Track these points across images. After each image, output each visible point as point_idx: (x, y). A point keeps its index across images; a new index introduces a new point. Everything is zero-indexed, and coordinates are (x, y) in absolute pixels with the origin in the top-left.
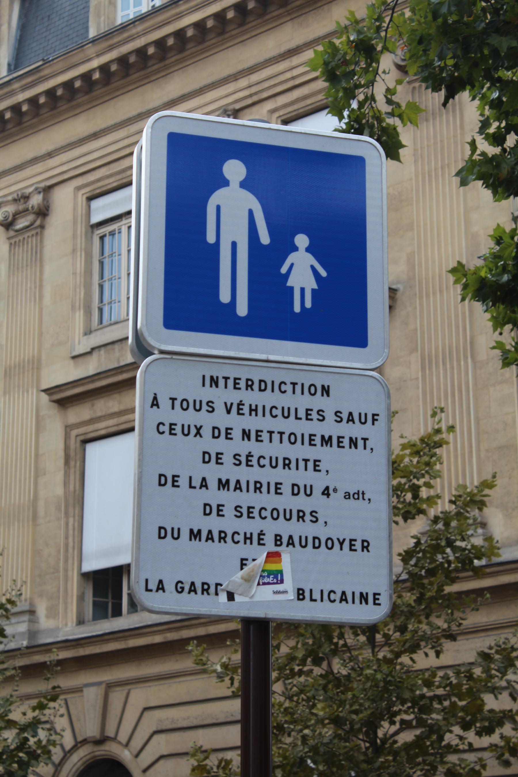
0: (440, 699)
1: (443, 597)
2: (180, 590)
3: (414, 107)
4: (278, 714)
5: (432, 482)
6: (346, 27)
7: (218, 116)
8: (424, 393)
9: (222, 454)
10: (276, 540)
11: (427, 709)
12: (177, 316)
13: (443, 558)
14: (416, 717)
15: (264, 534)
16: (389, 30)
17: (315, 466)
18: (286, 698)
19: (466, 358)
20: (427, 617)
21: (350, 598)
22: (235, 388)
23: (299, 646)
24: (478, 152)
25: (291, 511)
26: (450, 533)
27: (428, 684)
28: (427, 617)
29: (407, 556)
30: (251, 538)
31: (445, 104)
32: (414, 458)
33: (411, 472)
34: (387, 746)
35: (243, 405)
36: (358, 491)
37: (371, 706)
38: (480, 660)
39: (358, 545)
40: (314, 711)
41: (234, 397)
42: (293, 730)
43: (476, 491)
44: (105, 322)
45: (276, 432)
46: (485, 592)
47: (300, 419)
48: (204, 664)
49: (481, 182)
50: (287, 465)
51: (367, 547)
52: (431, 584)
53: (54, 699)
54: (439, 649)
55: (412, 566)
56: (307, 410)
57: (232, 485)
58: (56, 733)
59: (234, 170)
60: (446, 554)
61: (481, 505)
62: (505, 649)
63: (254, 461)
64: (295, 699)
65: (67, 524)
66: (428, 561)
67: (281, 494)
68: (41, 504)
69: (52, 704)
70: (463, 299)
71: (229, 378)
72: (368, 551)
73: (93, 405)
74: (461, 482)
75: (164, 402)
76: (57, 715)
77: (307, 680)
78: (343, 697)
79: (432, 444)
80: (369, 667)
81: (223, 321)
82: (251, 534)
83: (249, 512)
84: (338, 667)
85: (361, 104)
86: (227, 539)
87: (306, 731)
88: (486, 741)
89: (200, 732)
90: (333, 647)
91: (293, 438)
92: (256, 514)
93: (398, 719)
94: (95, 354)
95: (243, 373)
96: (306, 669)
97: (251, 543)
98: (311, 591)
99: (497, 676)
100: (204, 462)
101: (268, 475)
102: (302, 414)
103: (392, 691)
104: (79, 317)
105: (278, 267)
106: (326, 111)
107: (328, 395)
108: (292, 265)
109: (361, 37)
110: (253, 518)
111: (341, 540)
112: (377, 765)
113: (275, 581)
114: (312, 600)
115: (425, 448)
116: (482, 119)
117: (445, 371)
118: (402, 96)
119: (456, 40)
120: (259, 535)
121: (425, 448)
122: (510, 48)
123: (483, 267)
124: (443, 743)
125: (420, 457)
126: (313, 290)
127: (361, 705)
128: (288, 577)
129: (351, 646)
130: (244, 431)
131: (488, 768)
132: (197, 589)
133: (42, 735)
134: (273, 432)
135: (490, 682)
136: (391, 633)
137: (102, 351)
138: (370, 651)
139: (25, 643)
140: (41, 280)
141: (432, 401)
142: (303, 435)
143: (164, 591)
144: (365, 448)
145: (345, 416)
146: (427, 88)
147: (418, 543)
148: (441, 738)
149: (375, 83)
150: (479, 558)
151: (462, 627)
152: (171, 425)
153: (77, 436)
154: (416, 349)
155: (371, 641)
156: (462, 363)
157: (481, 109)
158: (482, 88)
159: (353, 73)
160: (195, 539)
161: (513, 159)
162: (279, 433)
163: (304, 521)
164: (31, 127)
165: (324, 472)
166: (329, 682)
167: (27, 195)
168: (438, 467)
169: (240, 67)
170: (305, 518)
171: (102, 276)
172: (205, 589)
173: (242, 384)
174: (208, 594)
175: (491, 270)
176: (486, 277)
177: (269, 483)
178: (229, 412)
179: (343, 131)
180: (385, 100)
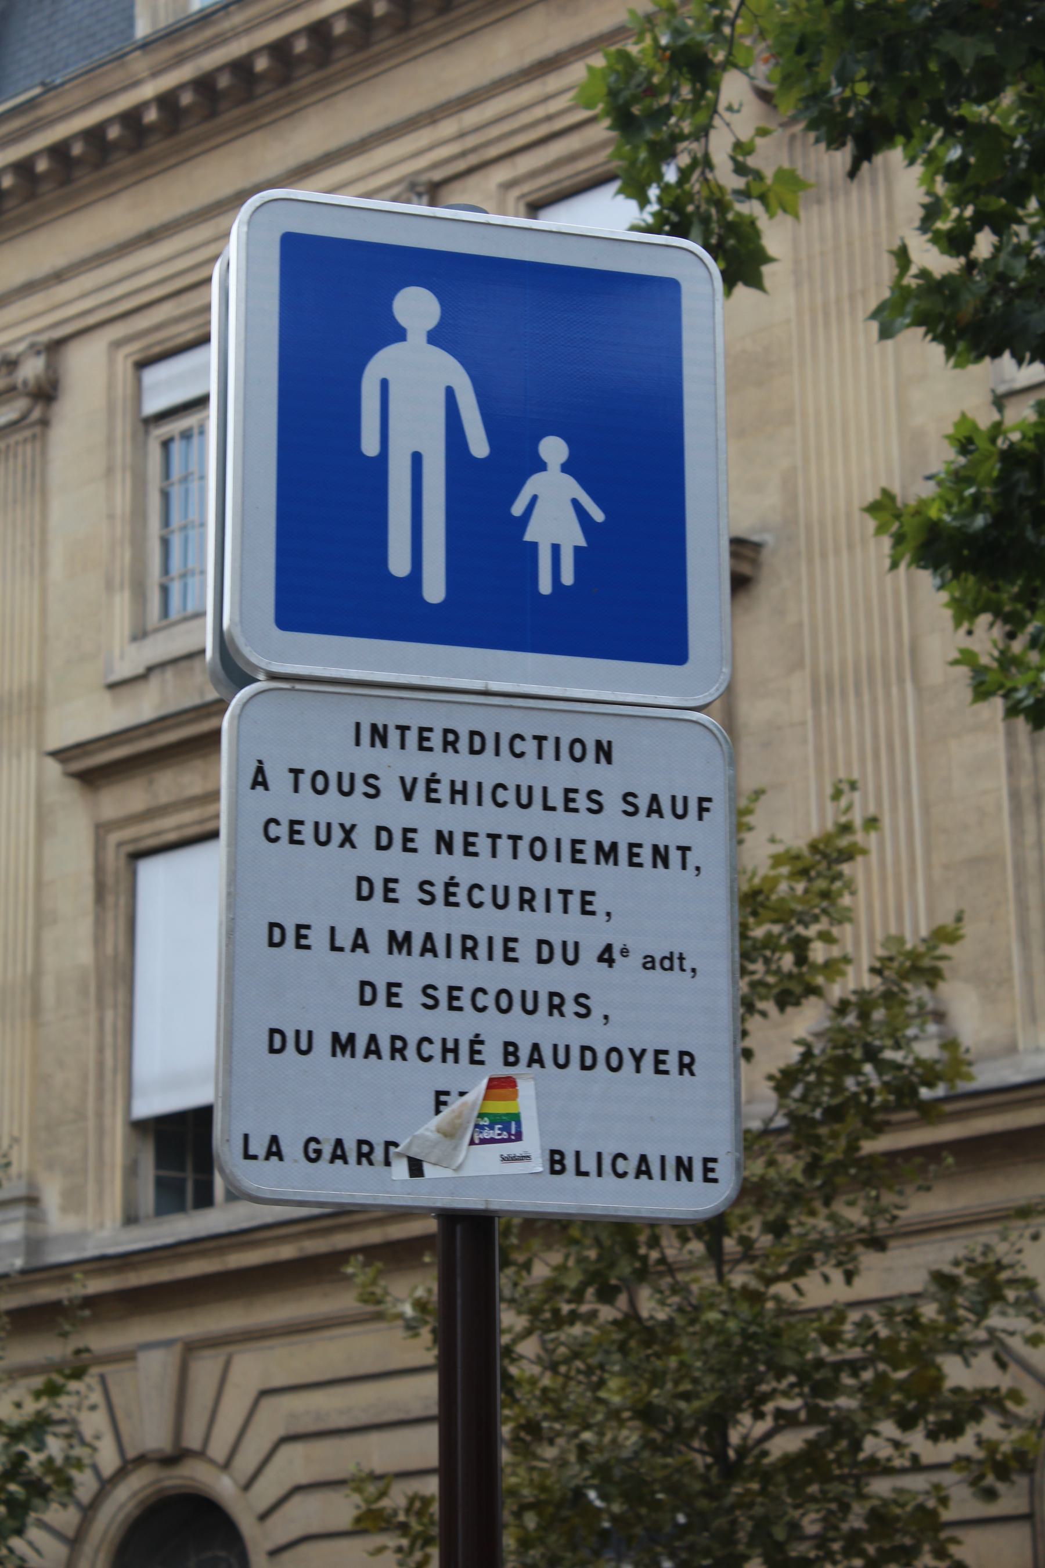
0: (854, 1367)
1: (858, 1162)
2: (313, 1156)
3: (789, 179)
4: (529, 1401)
5: (835, 931)
6: (649, 19)
7: (395, 199)
8: (819, 752)
9: (396, 881)
10: (507, 1054)
11: (829, 1388)
12: (301, 604)
13: (859, 1084)
14: (806, 1405)
15: (482, 1042)
16: (739, 22)
17: (584, 903)
18: (545, 1368)
19: (901, 680)
20: (827, 1203)
21: (655, 1169)
22: (421, 748)
23: (571, 1263)
24: (914, 270)
25: (536, 993)
26: (872, 1034)
27: (831, 1337)
28: (827, 1203)
29: (784, 1081)
30: (455, 1051)
31: (853, 173)
32: (798, 881)
33: (792, 913)
34: (749, 1461)
35: (438, 781)
36: (672, 953)
37: (718, 1385)
38: (933, 1288)
39: (672, 1062)
40: (602, 1394)
41: (419, 765)
42: (559, 1434)
43: (922, 949)
44: (175, 612)
45: (505, 837)
46: (944, 1154)
47: (553, 809)
48: (379, 1302)
49: (922, 330)
50: (527, 900)
51: (689, 1066)
52: (835, 1135)
53: (78, 1374)
54: (850, 1266)
55: (796, 1100)
56: (567, 791)
57: (417, 943)
58: (83, 1443)
59: (417, 307)
60: (864, 1074)
61: (932, 976)
62: (984, 1266)
63: (461, 896)
64: (563, 1369)
65: (101, 1022)
66: (827, 1090)
67: (516, 960)
68: (48, 983)
69: (73, 1385)
70: (894, 565)
71: (408, 728)
72: (692, 1074)
73: (151, 782)
74: (893, 931)
75: (278, 777)
76: (85, 1408)
77: (587, 1334)
78: (658, 1364)
79: (835, 855)
80: (712, 1306)
81: (392, 612)
82: (456, 1041)
83: (451, 998)
84: (650, 1306)
85: (684, 175)
86: (406, 1053)
87: (587, 1436)
88: (946, 1450)
89: (374, 1438)
90: (637, 1265)
91: (538, 848)
92: (465, 1001)
93: (769, 1407)
94: (154, 681)
95: (438, 717)
96: (584, 1308)
97: (456, 1061)
98: (578, 1154)
99: (968, 1320)
100: (360, 898)
101: (487, 923)
102: (556, 799)
103: (760, 1351)
104: (122, 604)
105: (510, 504)
106: (616, 185)
107: (609, 761)
108: (534, 499)
109: (682, 41)
110: (460, 1009)
111: (638, 1052)
112: (729, 1500)
113: (505, 1135)
114: (580, 1173)
115: (819, 862)
116: (927, 200)
117: (860, 707)
118: (768, 158)
119: (872, 45)
120: (472, 1043)
121: (819, 862)
122: (981, 60)
123: (933, 500)
124: (862, 1456)
125: (810, 880)
126: (577, 550)
127: (695, 1381)
128: (530, 1127)
129: (675, 1262)
130: (440, 834)
131: (952, 1504)
132: (348, 1154)
133: (55, 1446)
134: (499, 836)
135: (954, 1331)
136: (754, 1234)
137: (169, 674)
138: (712, 1271)
139: (19, 1263)
140: (44, 531)
141: (834, 768)
142: (558, 841)
143: (281, 1159)
144: (684, 867)
145: (643, 803)
146: (817, 141)
147: (807, 1055)
148: (856, 1446)
149: (713, 134)
150: (930, 1085)
151: (898, 1223)
152: (292, 823)
153: (120, 844)
154: (800, 664)
155: (715, 1252)
156: (894, 690)
157: (928, 181)
158: (928, 139)
159: (667, 111)
160: (343, 1053)
161: (984, 283)
162: (510, 837)
163: (562, 1014)
164: (22, 219)
165: (601, 916)
166: (631, 1335)
167: (13, 356)
168: (846, 900)
169: (442, 96)
170: (564, 1009)
171: (166, 521)
172: (365, 1153)
173: (436, 740)
174: (371, 1163)
175: (949, 505)
176: (940, 520)
177: (490, 939)
178: (408, 796)
179: (649, 230)
180: (730, 165)
